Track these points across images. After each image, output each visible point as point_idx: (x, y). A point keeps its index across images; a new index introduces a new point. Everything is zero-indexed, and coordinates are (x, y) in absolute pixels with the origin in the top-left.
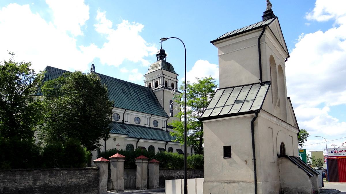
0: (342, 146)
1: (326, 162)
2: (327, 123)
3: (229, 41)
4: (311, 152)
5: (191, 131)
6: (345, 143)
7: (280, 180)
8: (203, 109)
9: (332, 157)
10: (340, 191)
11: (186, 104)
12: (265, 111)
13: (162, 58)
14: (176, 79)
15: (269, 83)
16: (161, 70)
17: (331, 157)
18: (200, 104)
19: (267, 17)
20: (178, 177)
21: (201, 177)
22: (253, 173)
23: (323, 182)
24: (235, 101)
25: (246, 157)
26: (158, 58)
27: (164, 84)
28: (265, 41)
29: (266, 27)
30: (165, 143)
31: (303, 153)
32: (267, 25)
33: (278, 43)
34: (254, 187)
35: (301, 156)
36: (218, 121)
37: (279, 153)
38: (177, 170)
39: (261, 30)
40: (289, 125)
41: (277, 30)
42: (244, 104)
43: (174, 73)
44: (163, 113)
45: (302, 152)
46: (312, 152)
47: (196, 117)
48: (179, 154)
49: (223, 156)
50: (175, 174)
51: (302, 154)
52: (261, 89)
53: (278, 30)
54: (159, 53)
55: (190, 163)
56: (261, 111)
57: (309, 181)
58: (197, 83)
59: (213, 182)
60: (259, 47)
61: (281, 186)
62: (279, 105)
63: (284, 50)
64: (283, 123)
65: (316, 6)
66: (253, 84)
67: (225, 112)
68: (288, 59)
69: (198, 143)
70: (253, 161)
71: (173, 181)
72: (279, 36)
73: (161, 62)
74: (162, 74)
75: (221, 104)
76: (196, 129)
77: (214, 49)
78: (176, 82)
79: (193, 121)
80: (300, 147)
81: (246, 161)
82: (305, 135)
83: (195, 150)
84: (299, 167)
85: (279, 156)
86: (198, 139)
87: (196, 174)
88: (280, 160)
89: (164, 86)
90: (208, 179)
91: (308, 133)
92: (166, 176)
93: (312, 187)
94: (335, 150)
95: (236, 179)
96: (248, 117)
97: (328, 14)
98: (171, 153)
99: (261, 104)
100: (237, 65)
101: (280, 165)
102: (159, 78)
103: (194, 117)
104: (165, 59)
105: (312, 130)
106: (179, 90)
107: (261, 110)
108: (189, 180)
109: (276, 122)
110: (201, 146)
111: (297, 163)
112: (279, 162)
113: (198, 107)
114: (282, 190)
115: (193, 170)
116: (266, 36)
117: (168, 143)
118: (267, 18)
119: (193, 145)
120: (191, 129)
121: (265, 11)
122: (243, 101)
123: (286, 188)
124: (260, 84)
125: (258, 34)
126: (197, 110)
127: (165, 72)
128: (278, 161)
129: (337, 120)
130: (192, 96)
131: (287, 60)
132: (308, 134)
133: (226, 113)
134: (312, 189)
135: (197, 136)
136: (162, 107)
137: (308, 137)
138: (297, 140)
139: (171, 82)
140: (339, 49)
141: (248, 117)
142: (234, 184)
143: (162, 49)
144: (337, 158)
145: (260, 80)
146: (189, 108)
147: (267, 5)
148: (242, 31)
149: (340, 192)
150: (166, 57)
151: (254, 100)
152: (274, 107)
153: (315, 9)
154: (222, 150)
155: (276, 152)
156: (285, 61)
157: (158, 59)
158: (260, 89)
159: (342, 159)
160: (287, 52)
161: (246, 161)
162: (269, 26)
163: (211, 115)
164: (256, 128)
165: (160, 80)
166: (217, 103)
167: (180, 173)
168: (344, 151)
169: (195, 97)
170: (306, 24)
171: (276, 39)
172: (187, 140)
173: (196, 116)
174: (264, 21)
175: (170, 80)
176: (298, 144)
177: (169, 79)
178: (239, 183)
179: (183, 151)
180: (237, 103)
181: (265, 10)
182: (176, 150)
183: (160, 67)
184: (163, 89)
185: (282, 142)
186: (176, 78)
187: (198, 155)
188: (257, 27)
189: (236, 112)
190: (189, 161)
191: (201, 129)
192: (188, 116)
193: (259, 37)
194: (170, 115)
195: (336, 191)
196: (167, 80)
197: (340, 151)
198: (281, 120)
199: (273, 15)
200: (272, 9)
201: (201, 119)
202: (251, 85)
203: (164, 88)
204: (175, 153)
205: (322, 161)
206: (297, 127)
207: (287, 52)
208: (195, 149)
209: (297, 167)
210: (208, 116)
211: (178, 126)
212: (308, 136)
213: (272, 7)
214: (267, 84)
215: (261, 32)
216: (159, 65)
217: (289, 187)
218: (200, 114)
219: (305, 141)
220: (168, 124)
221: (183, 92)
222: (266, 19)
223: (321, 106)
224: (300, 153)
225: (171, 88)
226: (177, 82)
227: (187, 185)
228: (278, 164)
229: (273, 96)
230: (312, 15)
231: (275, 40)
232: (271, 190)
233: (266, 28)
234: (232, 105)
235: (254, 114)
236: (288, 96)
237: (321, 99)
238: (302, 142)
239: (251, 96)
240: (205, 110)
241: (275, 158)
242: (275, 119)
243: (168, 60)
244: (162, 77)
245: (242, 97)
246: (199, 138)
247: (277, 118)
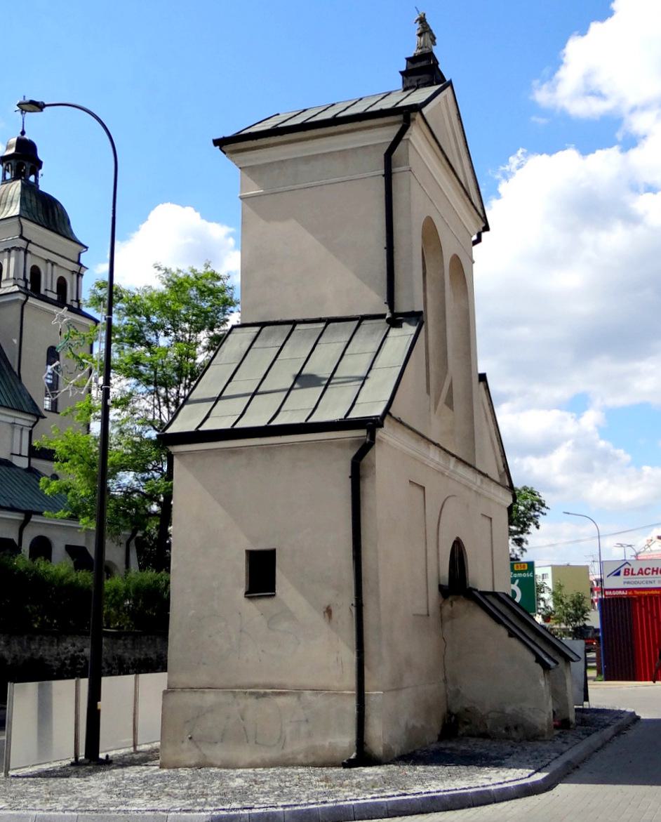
0: (649, 549)
1: (596, 604)
2: (596, 464)
3: (283, 146)
4: (550, 568)
5: (128, 478)
6: (655, 538)
7: (445, 680)
8: (178, 392)
9: (616, 590)
10: (637, 714)
11: (107, 368)
12: (401, 422)
13: (24, 174)
14: (79, 263)
15: (416, 318)
16: (16, 219)
17: (612, 590)
18: (169, 371)
19: (417, 78)
20: (68, 662)
21: (162, 671)
22: (350, 657)
23: (586, 679)
24: (298, 377)
25: (328, 596)
26: (5, 170)
27: (28, 277)
28: (407, 164)
29: (412, 115)
30: (19, 517)
31: (524, 575)
32: (417, 108)
33: (453, 176)
34: (355, 711)
35: (518, 585)
36: (232, 451)
37: (446, 581)
38: (60, 634)
39: (394, 123)
40: (482, 477)
41: (449, 129)
42: (327, 392)
43: (69, 236)
44: (16, 396)
45: (522, 572)
46: (555, 569)
47: (151, 423)
48: (78, 567)
49: (242, 590)
50: (54, 650)
51: (520, 579)
52: (388, 340)
53: (453, 128)
54: (12, 151)
55: (117, 605)
56: (386, 423)
57: (543, 683)
58: (159, 286)
59: (204, 692)
60: (388, 286)
61: (447, 704)
62: (450, 403)
63: (472, 204)
64: (462, 471)
65: (565, 60)
66: (361, 319)
67: (257, 418)
68: (484, 235)
69: (153, 527)
70: (354, 610)
71: (40, 687)
72: (455, 151)
73: (19, 190)
74: (21, 237)
75: (244, 384)
76: (148, 471)
77: (225, 167)
78: (75, 276)
79: (139, 435)
80: (517, 550)
81: (329, 611)
82: (533, 506)
83: (139, 553)
84: (511, 634)
85: (445, 592)
86: (155, 508)
87: (141, 649)
88: (448, 607)
89: (26, 288)
90: (183, 679)
91: (542, 499)
92: (15, 658)
93: (549, 707)
94: (627, 566)
95: (289, 681)
96: (340, 444)
97: (600, 95)
98: (42, 565)
99: (388, 397)
100: (309, 240)
101: (448, 624)
102: (7, 253)
103: (140, 421)
104: (36, 180)
105: (553, 490)
106: (85, 309)
107: (388, 417)
108: (106, 682)
109: (438, 464)
110: (164, 534)
111: (505, 621)
112: (446, 613)
113: (158, 382)
114: (453, 718)
115: (127, 634)
116: (414, 147)
117: (31, 517)
118: (418, 81)
119: (134, 532)
120: (124, 468)
121: (412, 55)
122: (325, 379)
123: (466, 710)
124: (388, 321)
125: (384, 134)
126: (156, 392)
127: (34, 231)
128: (441, 608)
129: (625, 457)
130: (136, 337)
131: (479, 240)
132: (543, 505)
133: (261, 421)
134: (550, 713)
135: (151, 497)
136: (16, 369)
137: (542, 513)
138: (507, 523)
139: (54, 274)
140: (631, 219)
141: (340, 444)
142: (280, 701)
143: (27, 137)
144: (630, 593)
145: (387, 306)
146: (120, 385)
147: (420, 35)
148: (328, 115)
149: (638, 718)
150: (40, 172)
151: (365, 378)
152: (432, 407)
153: (563, 73)
154: (242, 565)
155: (435, 575)
156: (475, 243)
157: (8, 176)
158: (385, 337)
159: (645, 597)
160: (480, 210)
161: (329, 611)
162: (425, 111)
163: (205, 427)
164: (366, 486)
165: (13, 260)
166: (230, 381)
167: (74, 645)
168: (653, 571)
169: (149, 345)
170: (533, 119)
171: (444, 160)
172: (108, 513)
173: (150, 417)
174: (408, 92)
175: (53, 264)
176: (510, 541)
177: (47, 261)
178: (299, 698)
179: (92, 551)
180: (303, 386)
181: (413, 51)
182: (63, 548)
183: (15, 210)
184: (21, 297)
185: (458, 538)
186: (76, 260)
187: (150, 575)
188: (381, 110)
189: (299, 419)
190: (114, 597)
191: (165, 469)
192: (113, 414)
193: (387, 148)
194: (47, 404)
195: (625, 716)
196: (42, 266)
197: (641, 569)
198: (453, 455)
199: (438, 74)
200: (437, 51)
201: (167, 441)
202: (356, 322)
203: (27, 296)
204: (60, 565)
205: (587, 604)
206: (508, 484)
207: (480, 210)
208: (141, 545)
209: (503, 632)
210: (193, 429)
211: (77, 456)
212: (544, 510)
213: (435, 44)
214: (410, 323)
215: (395, 130)
216: (9, 200)
217: (478, 707)
218: (164, 409)
219: (532, 528)
220: (35, 444)
221: (100, 316)
222: (416, 84)
223: (577, 405)
224: (515, 575)
225: (55, 297)
226: (79, 275)
227: (101, 705)
228: (442, 620)
229: (432, 367)
230: (553, 89)
231: (443, 165)
232: (412, 722)
233: (414, 119)
234: (285, 393)
235: (362, 433)
236: (481, 371)
237: (578, 382)
238: (522, 532)
239: (355, 364)
240: (186, 399)
241: (430, 600)
242: (434, 455)
243: (48, 182)
244: (18, 249)
245: (320, 365)
246: (159, 504)
247: (441, 447)
